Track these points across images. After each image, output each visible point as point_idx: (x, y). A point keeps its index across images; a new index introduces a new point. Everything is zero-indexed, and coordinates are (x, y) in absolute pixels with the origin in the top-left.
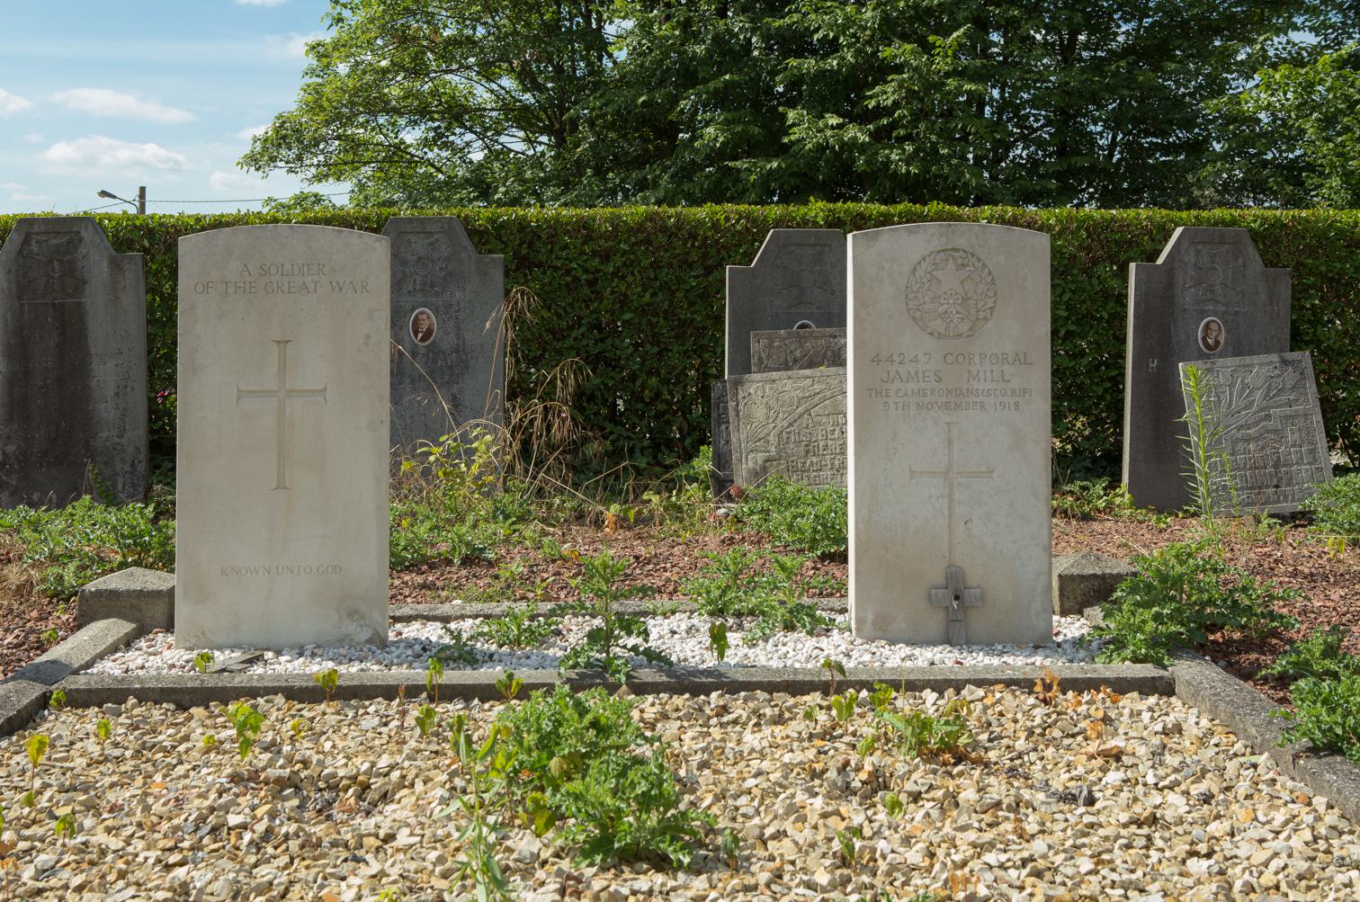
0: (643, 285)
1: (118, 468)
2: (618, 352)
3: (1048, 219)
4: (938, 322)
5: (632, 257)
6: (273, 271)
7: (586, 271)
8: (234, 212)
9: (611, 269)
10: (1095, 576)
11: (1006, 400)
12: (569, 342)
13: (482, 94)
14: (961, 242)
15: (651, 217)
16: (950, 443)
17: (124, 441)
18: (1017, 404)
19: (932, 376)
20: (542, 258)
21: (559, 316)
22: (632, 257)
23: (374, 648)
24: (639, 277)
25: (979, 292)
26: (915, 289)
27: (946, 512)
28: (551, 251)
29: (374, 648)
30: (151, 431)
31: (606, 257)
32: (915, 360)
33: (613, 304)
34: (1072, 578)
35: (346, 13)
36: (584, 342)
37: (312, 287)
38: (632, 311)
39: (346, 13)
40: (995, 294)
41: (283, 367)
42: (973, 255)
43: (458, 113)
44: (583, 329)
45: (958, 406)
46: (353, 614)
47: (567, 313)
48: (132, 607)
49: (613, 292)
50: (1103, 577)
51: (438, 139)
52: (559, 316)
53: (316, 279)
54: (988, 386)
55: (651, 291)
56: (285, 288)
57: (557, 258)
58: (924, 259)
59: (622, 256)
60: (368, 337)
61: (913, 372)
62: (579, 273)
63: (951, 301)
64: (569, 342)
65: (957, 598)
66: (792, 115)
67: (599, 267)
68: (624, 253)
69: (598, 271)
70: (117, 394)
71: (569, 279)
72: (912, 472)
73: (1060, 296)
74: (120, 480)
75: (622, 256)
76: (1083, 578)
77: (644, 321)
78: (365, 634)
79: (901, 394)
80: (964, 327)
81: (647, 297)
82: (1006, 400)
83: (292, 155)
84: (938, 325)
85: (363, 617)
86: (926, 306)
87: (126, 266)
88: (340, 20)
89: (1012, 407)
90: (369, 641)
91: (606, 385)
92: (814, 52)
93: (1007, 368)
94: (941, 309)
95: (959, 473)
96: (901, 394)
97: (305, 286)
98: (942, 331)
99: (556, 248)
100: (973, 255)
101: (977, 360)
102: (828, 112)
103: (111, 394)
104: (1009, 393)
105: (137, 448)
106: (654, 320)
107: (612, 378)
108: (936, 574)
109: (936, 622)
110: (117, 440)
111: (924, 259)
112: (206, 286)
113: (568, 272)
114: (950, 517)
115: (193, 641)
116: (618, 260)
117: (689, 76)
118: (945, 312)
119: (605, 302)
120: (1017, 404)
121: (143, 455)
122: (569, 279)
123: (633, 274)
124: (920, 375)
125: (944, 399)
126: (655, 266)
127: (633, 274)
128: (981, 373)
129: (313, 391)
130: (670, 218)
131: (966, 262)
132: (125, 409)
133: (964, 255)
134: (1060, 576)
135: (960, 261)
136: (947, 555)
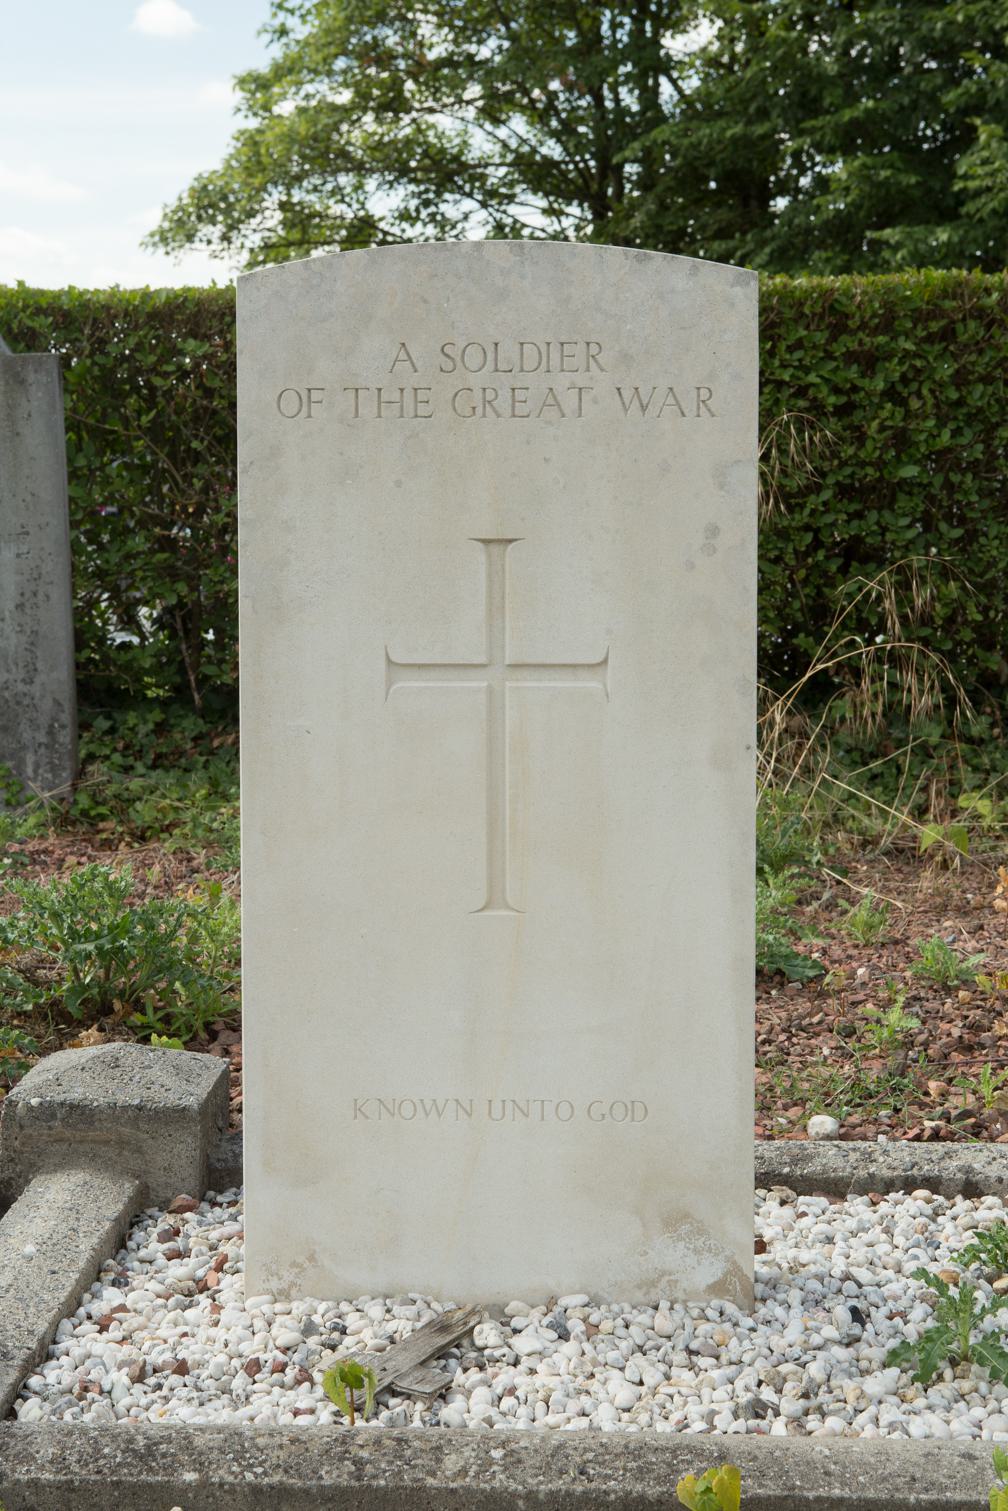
0: (938, 417)
1: (27, 736)
5: (918, 363)
6: (474, 357)
7: (836, 390)
8: (206, 284)
9: (880, 385)
13: (481, 144)
15: (953, 291)
17: (36, 689)
22: (918, 363)
23: (731, 1309)
24: (930, 401)
29: (731, 1309)
30: (78, 666)
31: (869, 362)
33: (885, 448)
35: (293, 22)
36: (829, 519)
37: (569, 401)
38: (916, 462)
39: (293, 22)
41: (495, 608)
43: (446, 171)
46: (676, 1221)
48: (122, 1143)
49: (882, 429)
53: (580, 379)
55: (952, 425)
56: (503, 403)
57: (784, 366)
59: (901, 362)
60: (713, 531)
67: (859, 383)
68: (907, 354)
69: (855, 389)
70: (20, 607)
74: (30, 759)
75: (901, 362)
77: (938, 480)
78: (708, 1272)
81: (946, 435)
83: (219, 229)
85: (701, 1231)
87: (31, 377)
88: (283, 32)
90: (718, 1288)
92: (828, 112)
97: (552, 399)
99: (782, 346)
103: (11, 606)
105: (57, 703)
106: (955, 478)
110: (21, 687)
112: (307, 398)
113: (802, 392)
115: (288, 1276)
116: (895, 369)
119: (869, 445)
121: (66, 717)
123: (919, 395)
126: (960, 379)
127: (919, 395)
129: (574, 666)
130: (988, 291)
132: (35, 633)
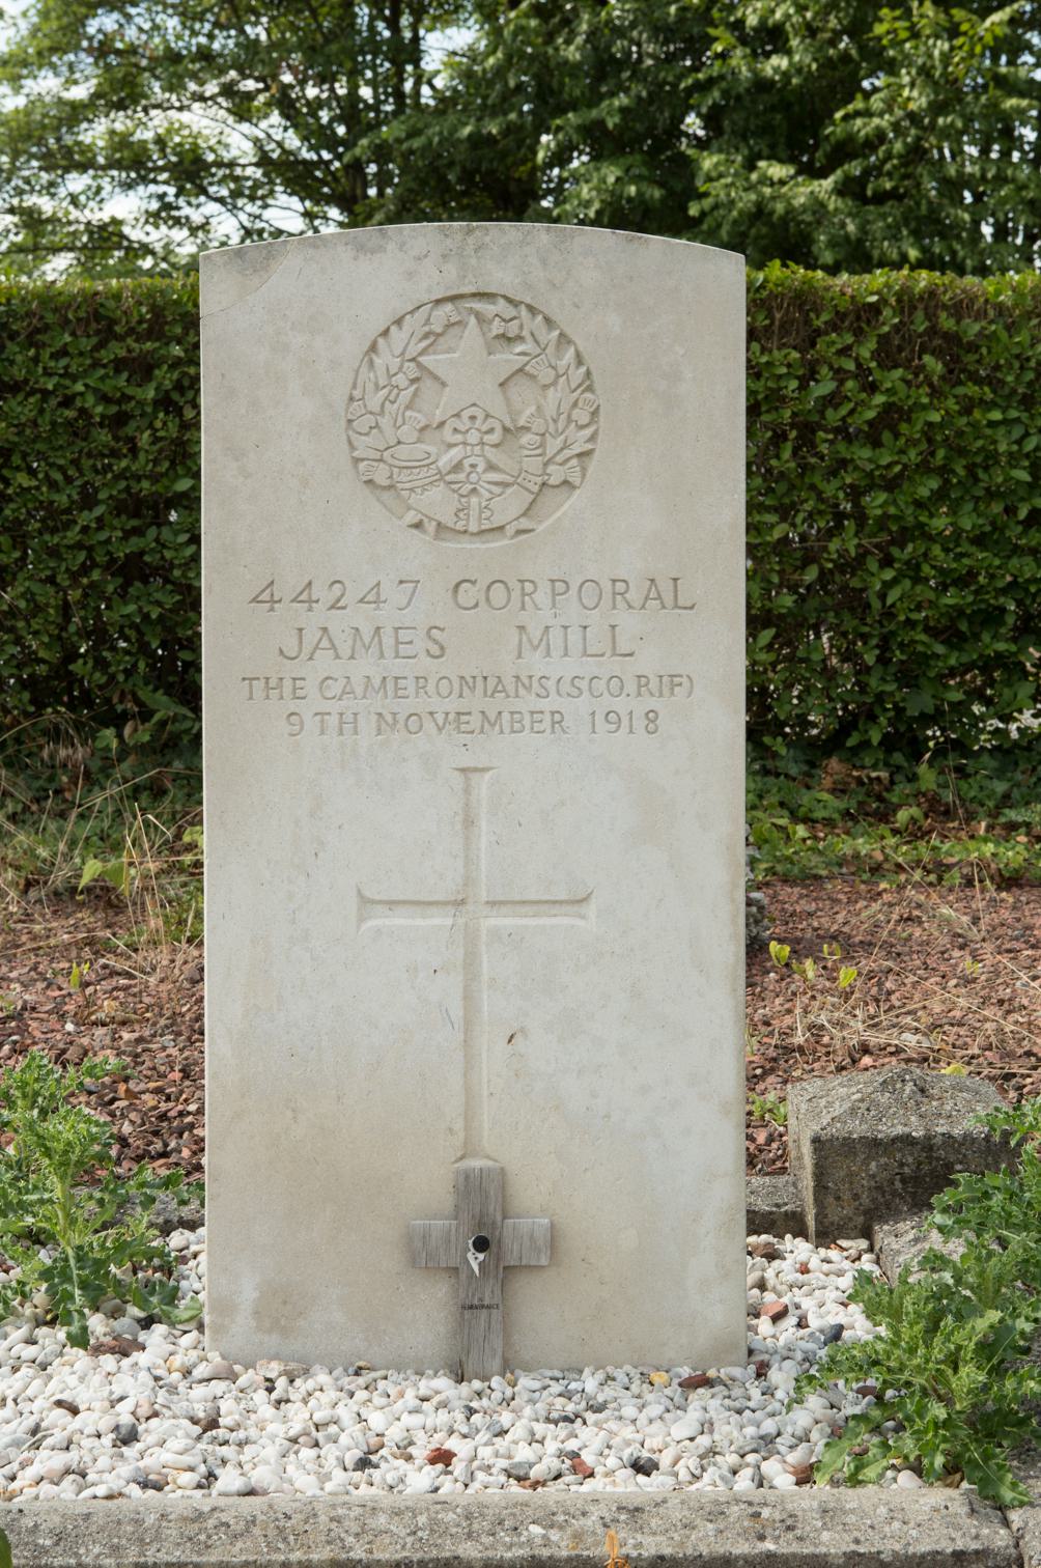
2: (168, 554)
3: (998, 293)
4: (437, 493)
7: (105, 399)
10: (907, 1140)
11: (620, 705)
12: (73, 535)
13: (238, 142)
14: (500, 277)
16: (469, 822)
18: (651, 716)
19: (421, 644)
20: (19, 373)
21: (53, 485)
25: (550, 410)
26: (374, 402)
27: (457, 1012)
28: (36, 360)
32: (373, 597)
34: (848, 1146)
36: (103, 536)
40: (595, 413)
42: (532, 309)
43: (192, 170)
44: (99, 511)
45: (489, 721)
47: (69, 480)
49: (156, 440)
50: (927, 1145)
51: (163, 214)
52: (53, 485)
54: (571, 667)
57: (48, 373)
58: (399, 322)
61: (367, 633)
62: (90, 400)
63: (473, 437)
64: (73, 535)
65: (481, 1244)
66: (708, 162)
67: (130, 391)
71: (70, 414)
72: (364, 901)
73: (1019, 442)
76: (874, 1145)
79: (336, 688)
80: (507, 508)
82: (620, 705)
84: (437, 502)
86: (403, 452)
89: (640, 724)
91: (146, 617)
93: (629, 623)
94: (446, 459)
95: (492, 904)
96: (336, 688)
98: (449, 520)
100: (532, 309)
101: (542, 597)
102: (761, 158)
104: (631, 687)
107: (159, 603)
108: (426, 1187)
109: (427, 1313)
111: (399, 322)
113: (67, 402)
114: (468, 1025)
117: (550, 102)
118: (457, 467)
119: (142, 456)
120: (651, 716)
122: (70, 414)
124: (388, 641)
125: (453, 705)
128: (556, 636)
131: (513, 329)
133: (510, 312)
134: (816, 1140)
135: (497, 328)
136: (459, 1125)
